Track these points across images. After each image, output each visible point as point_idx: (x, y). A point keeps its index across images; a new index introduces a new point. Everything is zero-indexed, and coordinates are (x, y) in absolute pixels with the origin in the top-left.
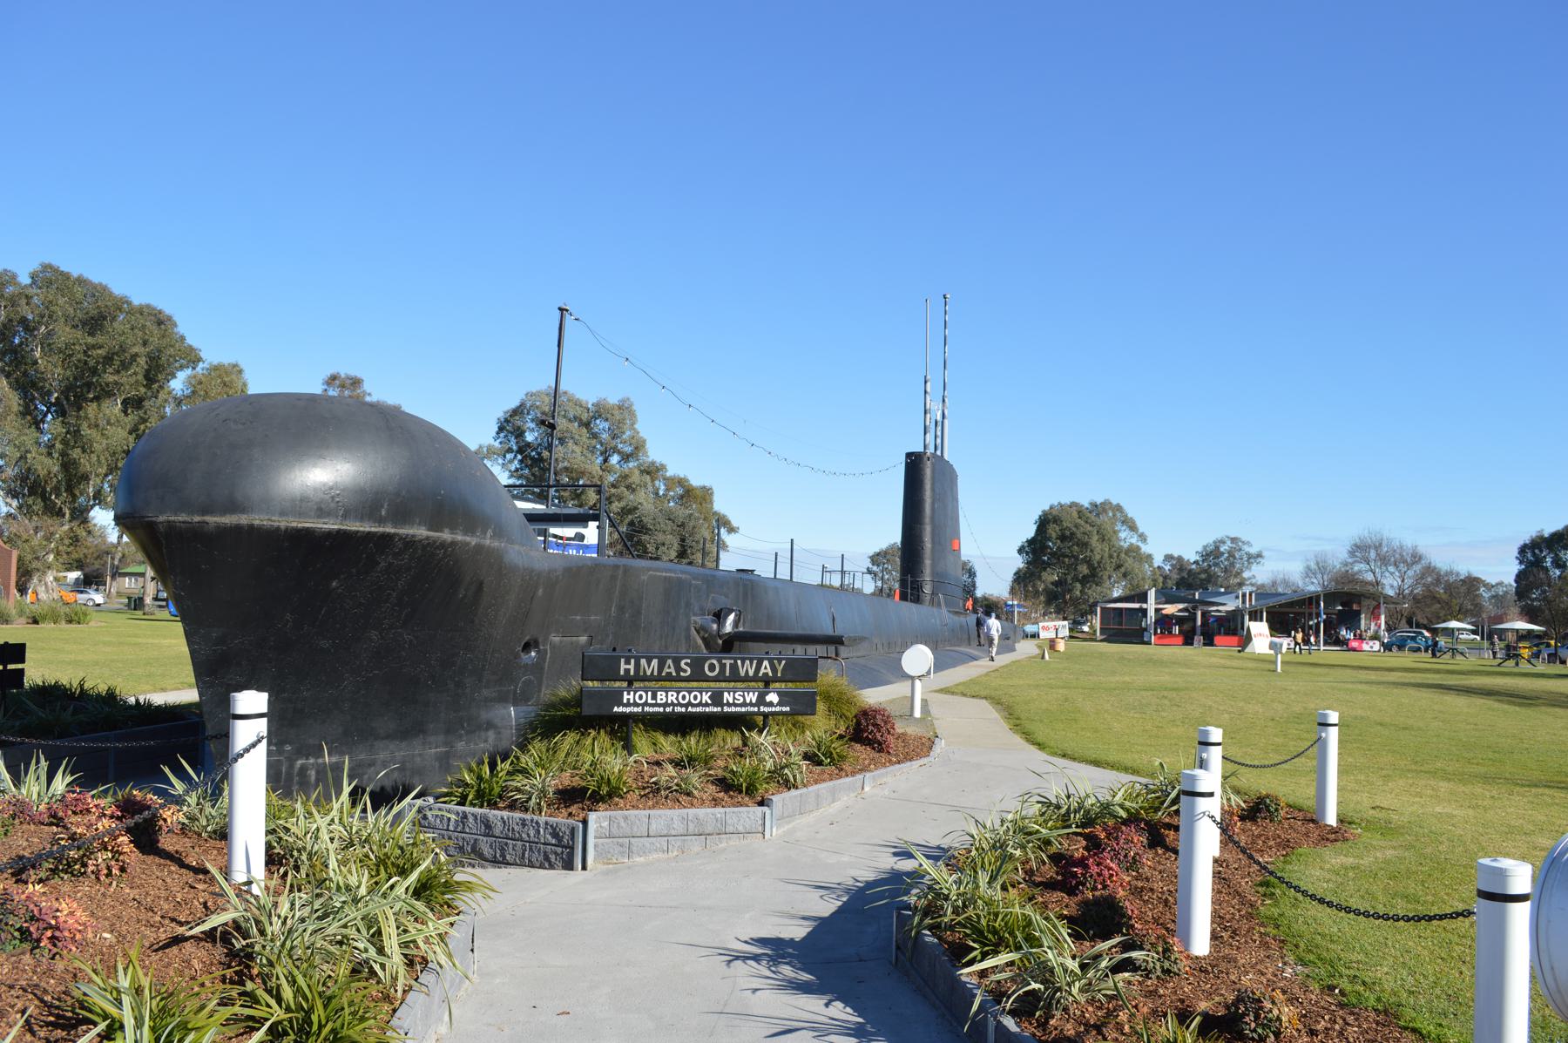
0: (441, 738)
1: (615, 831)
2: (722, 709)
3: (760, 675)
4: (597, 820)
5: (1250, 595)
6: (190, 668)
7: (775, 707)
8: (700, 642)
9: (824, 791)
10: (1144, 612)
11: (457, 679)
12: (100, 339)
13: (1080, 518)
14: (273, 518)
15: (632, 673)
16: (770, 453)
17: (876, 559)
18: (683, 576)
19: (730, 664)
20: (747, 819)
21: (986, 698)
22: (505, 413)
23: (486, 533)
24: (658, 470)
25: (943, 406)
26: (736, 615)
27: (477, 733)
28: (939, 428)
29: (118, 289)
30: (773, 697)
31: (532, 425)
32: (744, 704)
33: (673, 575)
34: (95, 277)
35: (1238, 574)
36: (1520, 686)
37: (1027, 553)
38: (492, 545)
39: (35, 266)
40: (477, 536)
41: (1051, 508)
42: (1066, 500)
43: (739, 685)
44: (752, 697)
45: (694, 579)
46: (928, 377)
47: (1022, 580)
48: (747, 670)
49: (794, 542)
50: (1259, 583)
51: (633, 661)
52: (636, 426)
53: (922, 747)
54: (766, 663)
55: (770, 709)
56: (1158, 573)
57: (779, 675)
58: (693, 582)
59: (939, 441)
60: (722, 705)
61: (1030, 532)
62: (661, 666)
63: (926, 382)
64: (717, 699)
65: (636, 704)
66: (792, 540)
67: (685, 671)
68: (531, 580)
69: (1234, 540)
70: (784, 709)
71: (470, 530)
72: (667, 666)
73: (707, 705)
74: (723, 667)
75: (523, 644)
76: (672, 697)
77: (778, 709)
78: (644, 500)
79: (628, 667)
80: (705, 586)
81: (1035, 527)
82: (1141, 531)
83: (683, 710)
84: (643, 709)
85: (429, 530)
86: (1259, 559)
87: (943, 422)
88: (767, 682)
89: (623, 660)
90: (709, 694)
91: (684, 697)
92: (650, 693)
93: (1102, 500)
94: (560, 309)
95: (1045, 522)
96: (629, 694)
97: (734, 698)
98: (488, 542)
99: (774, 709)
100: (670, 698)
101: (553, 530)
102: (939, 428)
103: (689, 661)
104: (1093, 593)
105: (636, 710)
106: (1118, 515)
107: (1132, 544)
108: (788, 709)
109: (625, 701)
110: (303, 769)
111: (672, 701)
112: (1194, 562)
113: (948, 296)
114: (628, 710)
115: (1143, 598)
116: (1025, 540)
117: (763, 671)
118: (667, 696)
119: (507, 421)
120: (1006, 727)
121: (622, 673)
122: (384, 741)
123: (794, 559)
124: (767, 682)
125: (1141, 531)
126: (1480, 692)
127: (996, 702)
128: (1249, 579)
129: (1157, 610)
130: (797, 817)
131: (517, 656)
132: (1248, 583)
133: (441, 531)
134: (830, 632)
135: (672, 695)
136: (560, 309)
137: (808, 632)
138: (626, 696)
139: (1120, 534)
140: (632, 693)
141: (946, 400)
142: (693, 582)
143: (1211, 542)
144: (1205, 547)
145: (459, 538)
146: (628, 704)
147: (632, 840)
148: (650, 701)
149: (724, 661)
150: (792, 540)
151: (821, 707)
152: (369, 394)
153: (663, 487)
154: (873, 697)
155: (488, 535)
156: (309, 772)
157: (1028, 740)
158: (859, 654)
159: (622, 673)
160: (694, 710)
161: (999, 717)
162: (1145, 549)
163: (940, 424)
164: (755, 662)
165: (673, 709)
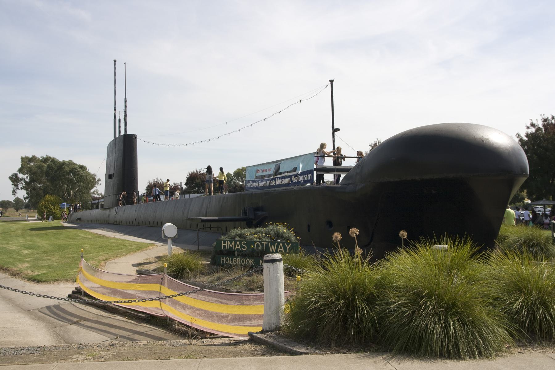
16: (327, 86)
19: (266, 244)
36: (490, 139)
48: (273, 249)
71: (369, 261)
96: (223, 259)
149: (263, 243)
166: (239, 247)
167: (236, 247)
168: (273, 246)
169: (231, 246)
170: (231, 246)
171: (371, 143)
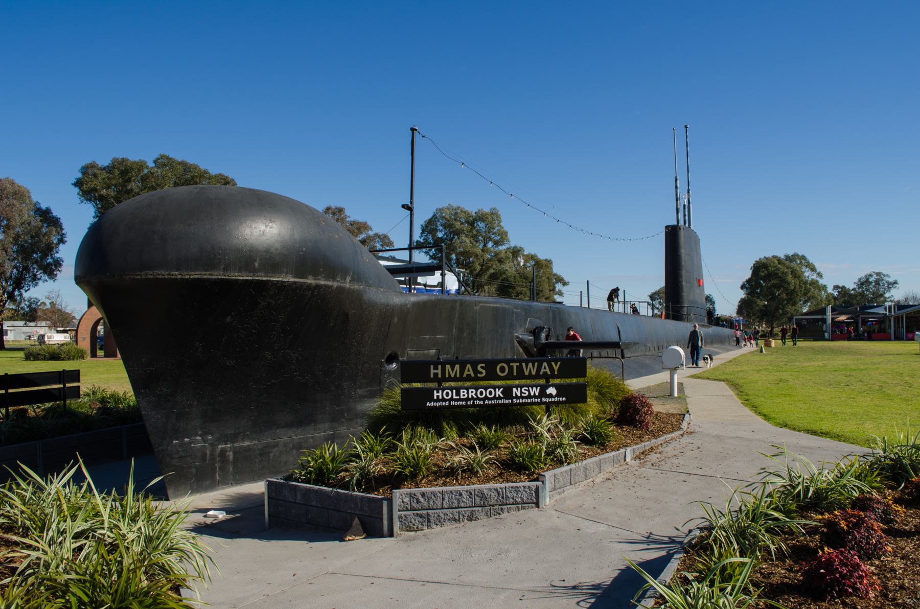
0: (327, 425)
1: (415, 505)
2: (512, 401)
3: (541, 373)
4: (400, 496)
5: (894, 307)
6: (130, 383)
7: (554, 398)
8: (521, 350)
9: (591, 465)
10: (824, 321)
11: (337, 383)
12: (139, 178)
13: (779, 263)
14: (172, 273)
15: (440, 376)
17: (652, 297)
18: (507, 306)
19: (517, 366)
20: (524, 493)
21: (723, 380)
22: (425, 222)
23: (345, 279)
24: (519, 251)
25: (689, 195)
27: (355, 420)
28: (686, 210)
29: (203, 167)
30: (552, 391)
31: (441, 228)
32: (529, 397)
33: (498, 305)
34: (191, 161)
35: (882, 295)
37: (747, 289)
38: (352, 287)
39: (156, 155)
40: (338, 281)
41: (760, 259)
42: (769, 255)
43: (523, 382)
44: (535, 391)
45: (515, 308)
47: (744, 307)
49: (590, 282)
50: (896, 300)
51: (440, 367)
52: (501, 224)
53: (674, 422)
54: (545, 364)
55: (550, 400)
56: (831, 296)
57: (556, 373)
58: (515, 310)
59: (687, 218)
60: (512, 398)
61: (748, 274)
62: (462, 370)
64: (507, 392)
65: (444, 400)
66: (588, 281)
67: (481, 373)
68: (388, 313)
69: (878, 274)
70: (561, 399)
72: (467, 369)
73: (500, 398)
74: (511, 368)
75: (386, 357)
76: (472, 393)
77: (556, 399)
78: (509, 268)
79: (436, 371)
80: (523, 313)
81: (751, 271)
82: (818, 271)
83: (482, 402)
84: (450, 403)
85: (295, 277)
86: (895, 285)
88: (547, 377)
89: (432, 367)
90: (501, 389)
91: (481, 393)
92: (454, 391)
93: (792, 253)
95: (760, 268)
97: (521, 392)
98: (347, 285)
99: (553, 400)
100: (470, 394)
101: (420, 279)
102: (686, 210)
103: (484, 365)
104: (790, 309)
105: (444, 404)
106: (803, 261)
107: (813, 279)
108: (564, 399)
109: (435, 398)
110: (223, 453)
111: (472, 396)
112: (853, 290)
114: (438, 404)
115: (823, 311)
116: (745, 280)
117: (543, 370)
118: (468, 393)
119: (426, 226)
120: (739, 401)
121: (432, 376)
122: (284, 429)
123: (590, 294)
124: (547, 377)
125: (818, 271)
127: (736, 386)
128: (889, 298)
129: (833, 319)
130: (568, 487)
131: (381, 364)
132: (888, 300)
133: (306, 278)
134: (615, 338)
135: (472, 392)
137: (601, 340)
138: (436, 394)
139: (805, 274)
140: (440, 391)
142: (515, 310)
143: (864, 276)
144: (860, 279)
145: (322, 282)
146: (438, 400)
147: (429, 511)
148: (455, 397)
150: (588, 281)
151: (591, 394)
152: (349, 217)
153: (522, 261)
154: (635, 385)
155: (348, 279)
156: (228, 453)
157: (756, 412)
158: (638, 354)
159: (432, 376)
160: (490, 402)
161: (734, 394)
162: (821, 282)
163: (686, 207)
164: (536, 364)
165: (474, 402)
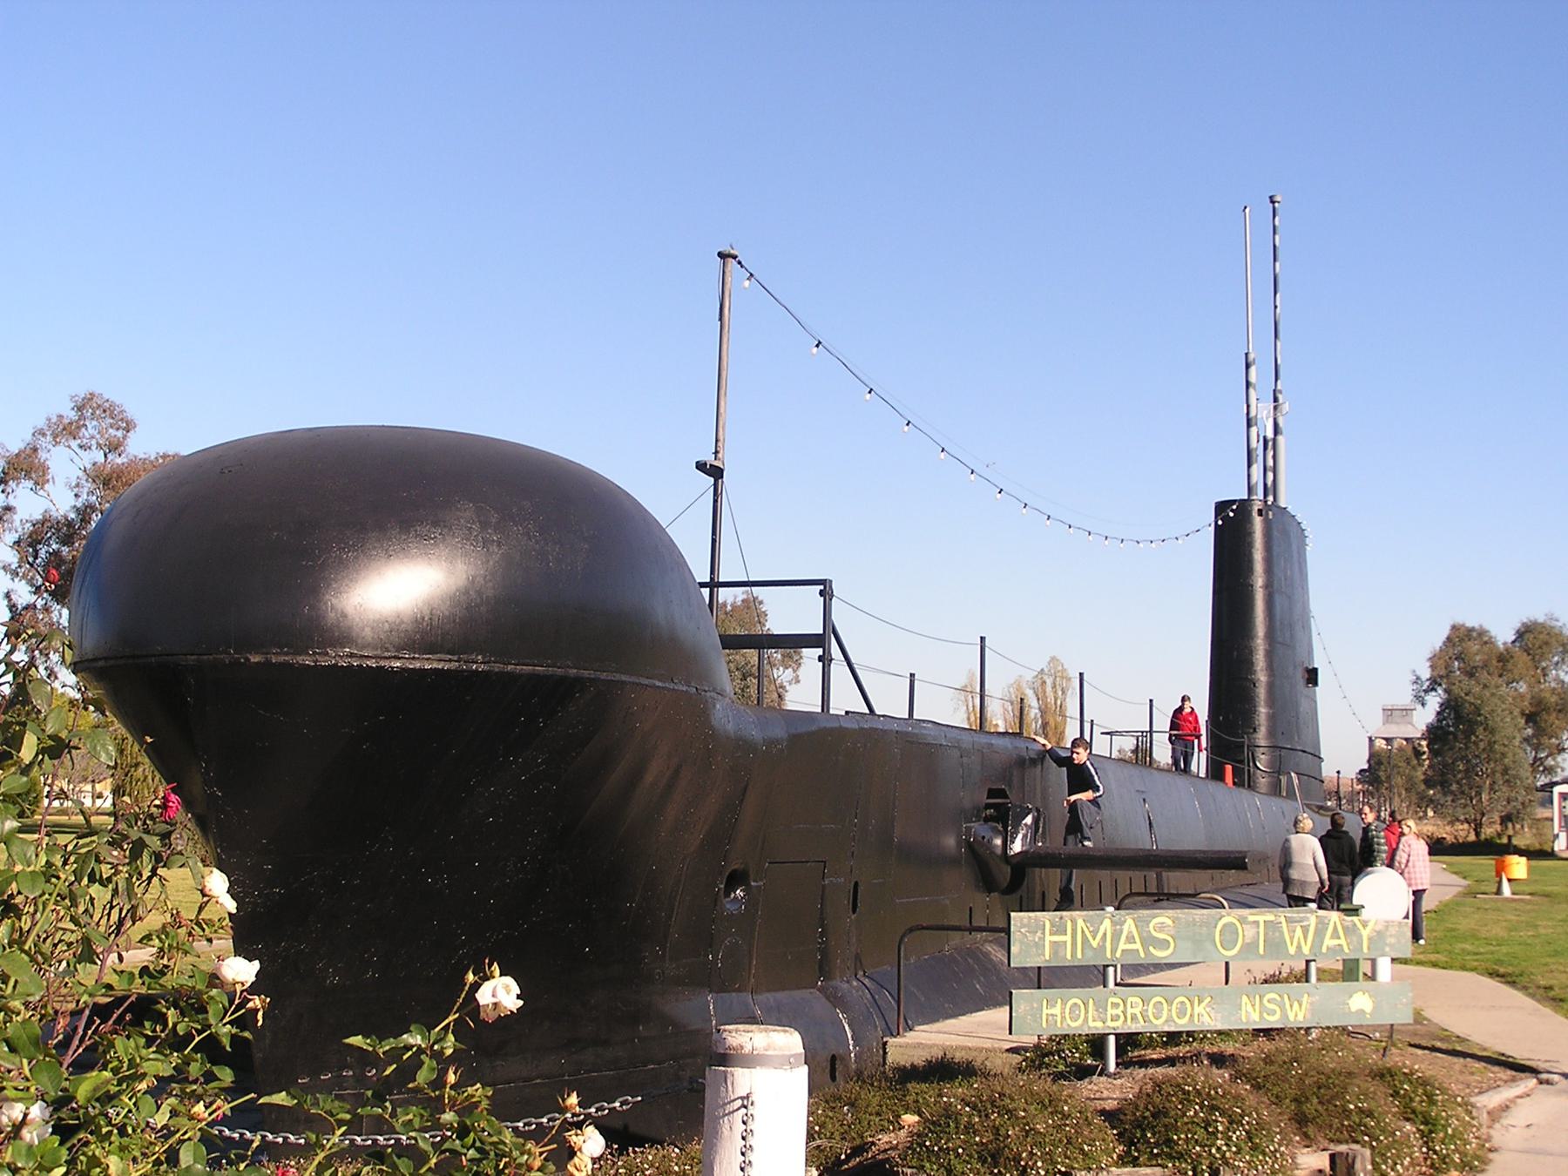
23: (442, 638)
26: (1033, 817)
28: (1270, 453)
46: (1251, 357)
63: (1248, 366)
87: (1274, 440)
94: (720, 255)
102: (1270, 453)
113: (1278, 198)
126: (1176, 880)
136: (720, 255)
141: (1280, 397)
163: (1270, 444)
166: (1138, 946)
167: (1122, 946)
168: (1296, 1005)
169: (1095, 944)
170: (1095, 944)
171: (1434, 648)
